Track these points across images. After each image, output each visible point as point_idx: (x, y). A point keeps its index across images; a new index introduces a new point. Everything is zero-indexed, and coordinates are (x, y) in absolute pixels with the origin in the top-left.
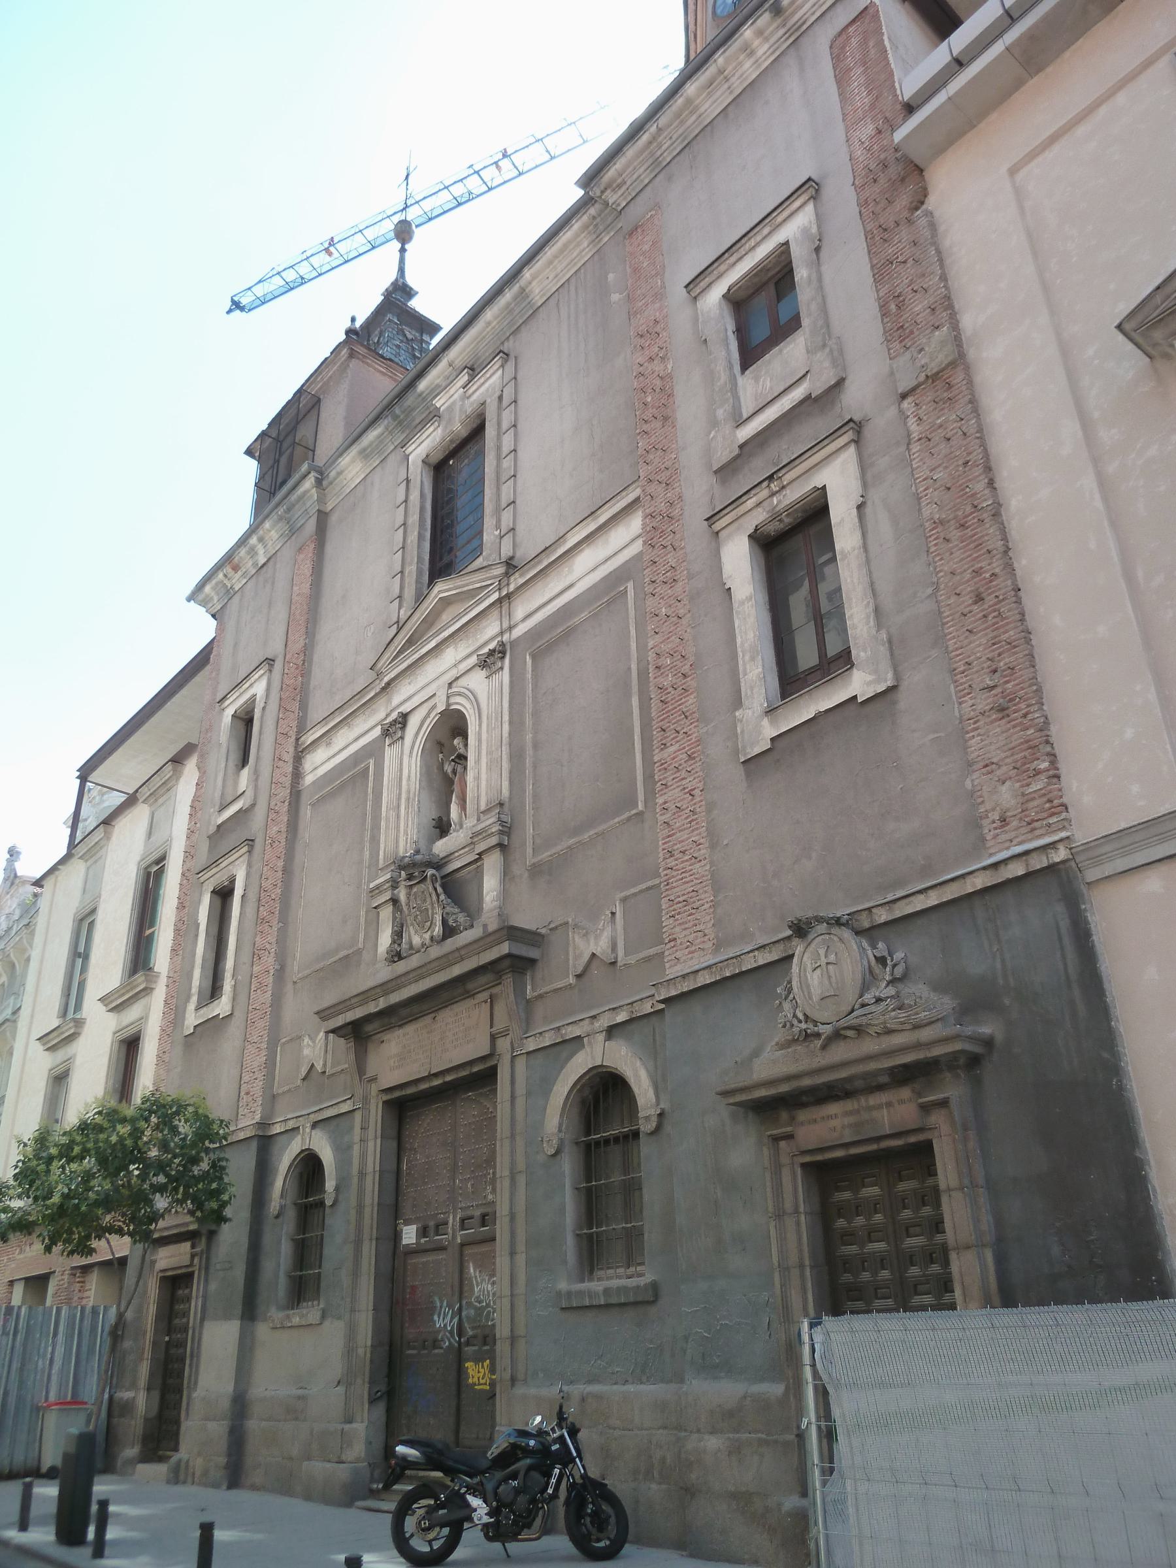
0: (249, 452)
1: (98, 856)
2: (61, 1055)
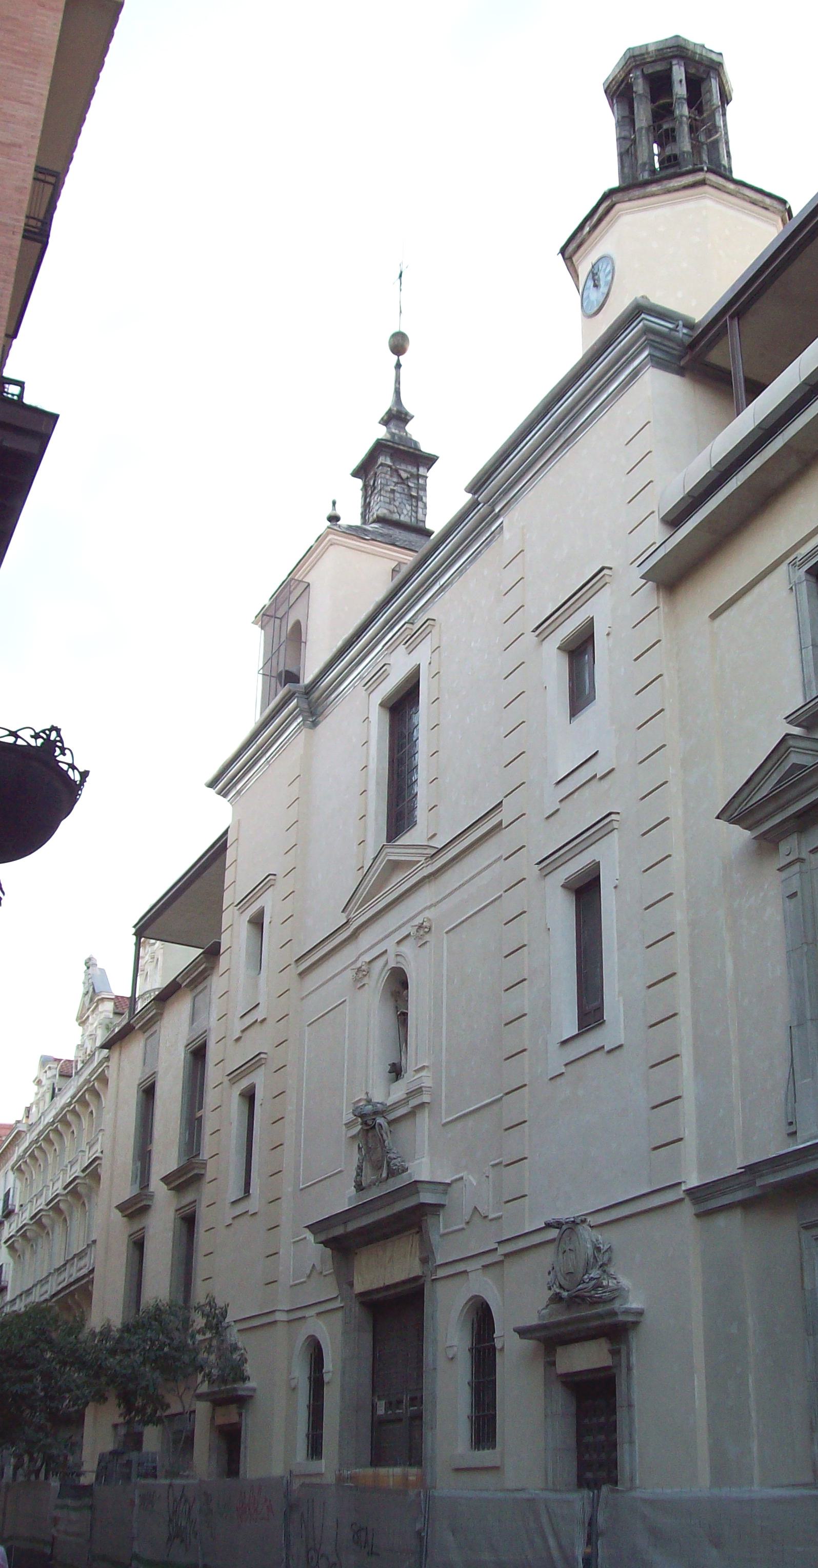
0: (255, 623)
1: (200, 987)
2: (189, 1197)
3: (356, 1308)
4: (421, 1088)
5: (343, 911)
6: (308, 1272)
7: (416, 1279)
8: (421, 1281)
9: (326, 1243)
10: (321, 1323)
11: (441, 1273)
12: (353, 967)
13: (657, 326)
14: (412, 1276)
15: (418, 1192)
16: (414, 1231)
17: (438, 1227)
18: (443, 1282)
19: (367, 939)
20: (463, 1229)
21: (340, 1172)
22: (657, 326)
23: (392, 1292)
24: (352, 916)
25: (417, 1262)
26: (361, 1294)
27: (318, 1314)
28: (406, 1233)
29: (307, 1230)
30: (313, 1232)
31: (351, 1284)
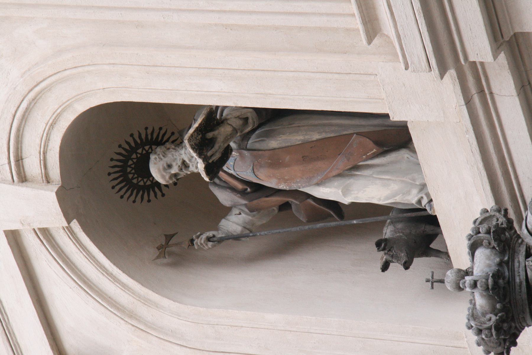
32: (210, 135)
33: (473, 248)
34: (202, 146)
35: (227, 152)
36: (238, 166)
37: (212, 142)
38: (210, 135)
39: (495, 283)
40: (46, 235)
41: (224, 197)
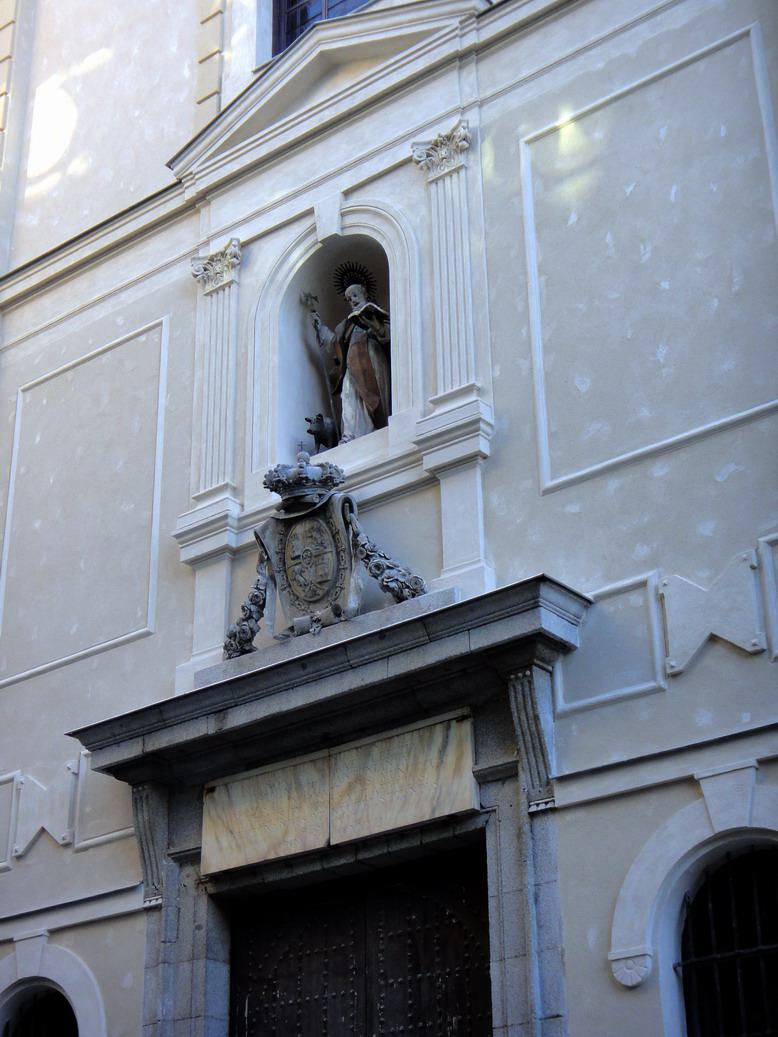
3: (199, 911)
4: (477, 421)
5: (170, 165)
6: (20, 847)
7: (471, 815)
8: (479, 822)
9: (116, 771)
10: (57, 946)
11: (563, 796)
12: (201, 254)
13: (288, 119)
14: (446, 810)
15: (536, 606)
16: (458, 713)
17: (551, 694)
18: (570, 817)
19: (227, 210)
20: (660, 690)
21: (148, 634)
22: (288, 119)
23: (415, 842)
24: (194, 168)
25: (468, 781)
26: (217, 878)
27: (55, 932)
28: (313, 756)
29: (76, 741)
30: (87, 745)
31: (193, 857)
32: (374, 317)
33: (321, 466)
34: (368, 313)
35: (365, 327)
36: (357, 333)
37: (371, 319)
38: (374, 317)
39: (303, 478)
40: (313, 229)
41: (340, 327)
